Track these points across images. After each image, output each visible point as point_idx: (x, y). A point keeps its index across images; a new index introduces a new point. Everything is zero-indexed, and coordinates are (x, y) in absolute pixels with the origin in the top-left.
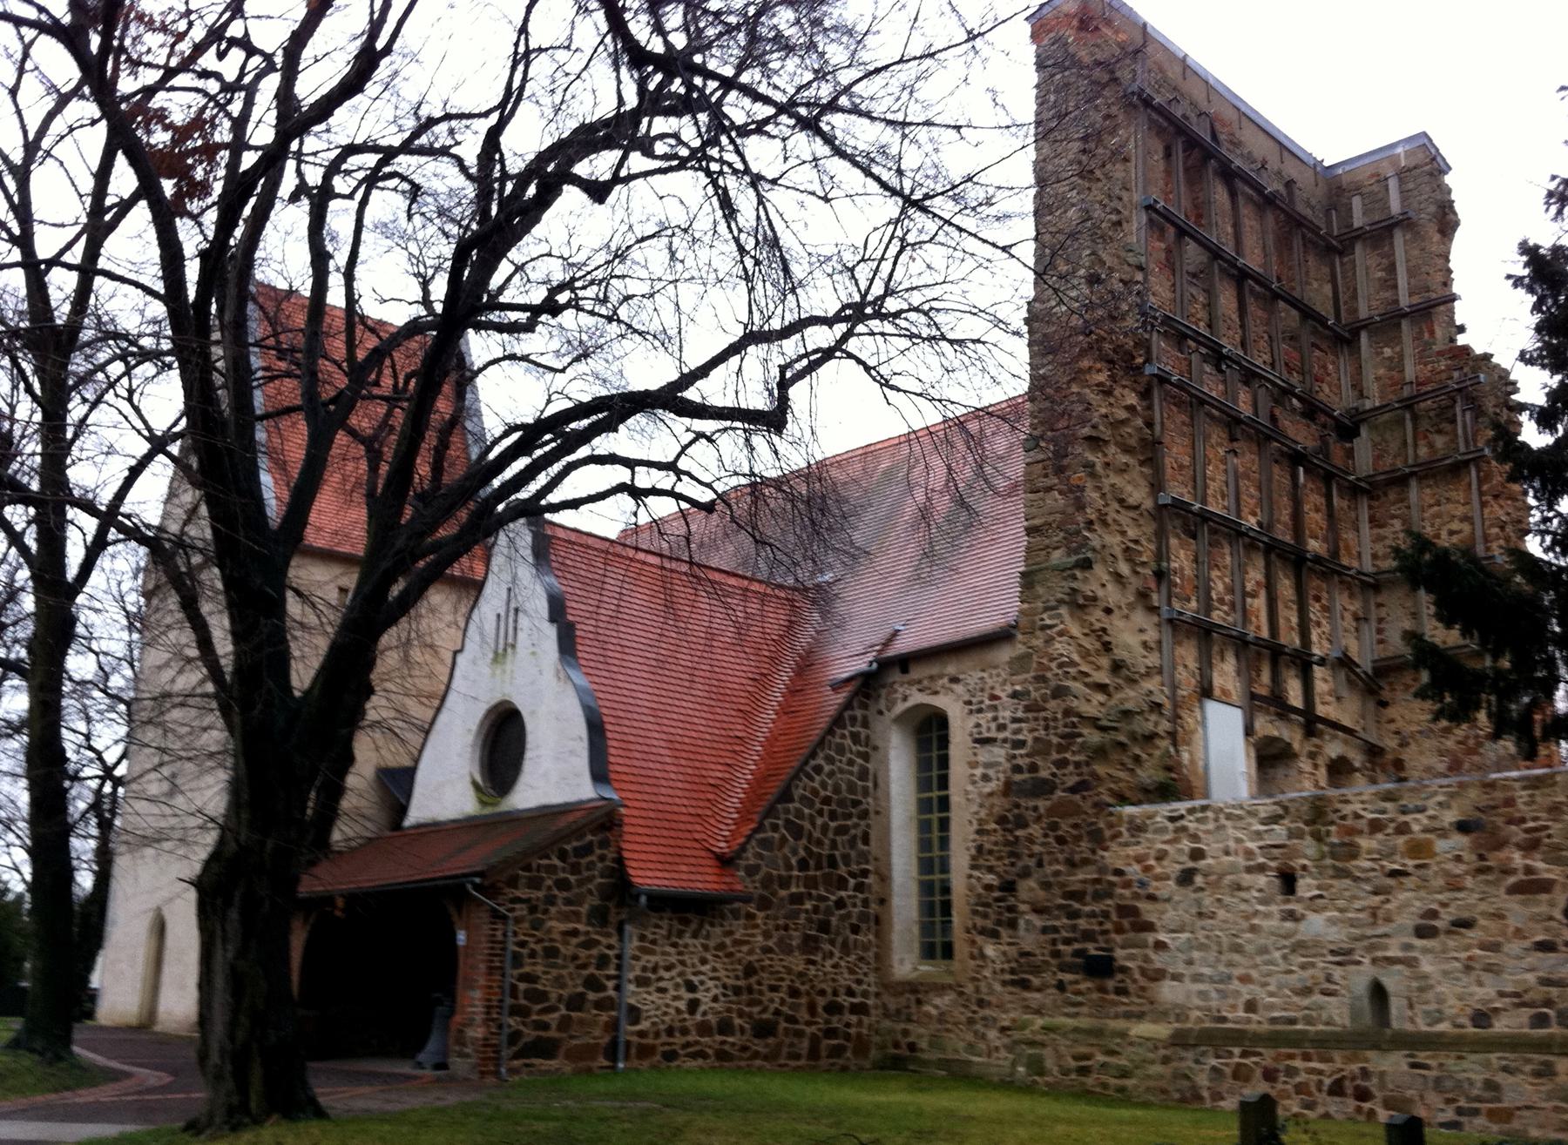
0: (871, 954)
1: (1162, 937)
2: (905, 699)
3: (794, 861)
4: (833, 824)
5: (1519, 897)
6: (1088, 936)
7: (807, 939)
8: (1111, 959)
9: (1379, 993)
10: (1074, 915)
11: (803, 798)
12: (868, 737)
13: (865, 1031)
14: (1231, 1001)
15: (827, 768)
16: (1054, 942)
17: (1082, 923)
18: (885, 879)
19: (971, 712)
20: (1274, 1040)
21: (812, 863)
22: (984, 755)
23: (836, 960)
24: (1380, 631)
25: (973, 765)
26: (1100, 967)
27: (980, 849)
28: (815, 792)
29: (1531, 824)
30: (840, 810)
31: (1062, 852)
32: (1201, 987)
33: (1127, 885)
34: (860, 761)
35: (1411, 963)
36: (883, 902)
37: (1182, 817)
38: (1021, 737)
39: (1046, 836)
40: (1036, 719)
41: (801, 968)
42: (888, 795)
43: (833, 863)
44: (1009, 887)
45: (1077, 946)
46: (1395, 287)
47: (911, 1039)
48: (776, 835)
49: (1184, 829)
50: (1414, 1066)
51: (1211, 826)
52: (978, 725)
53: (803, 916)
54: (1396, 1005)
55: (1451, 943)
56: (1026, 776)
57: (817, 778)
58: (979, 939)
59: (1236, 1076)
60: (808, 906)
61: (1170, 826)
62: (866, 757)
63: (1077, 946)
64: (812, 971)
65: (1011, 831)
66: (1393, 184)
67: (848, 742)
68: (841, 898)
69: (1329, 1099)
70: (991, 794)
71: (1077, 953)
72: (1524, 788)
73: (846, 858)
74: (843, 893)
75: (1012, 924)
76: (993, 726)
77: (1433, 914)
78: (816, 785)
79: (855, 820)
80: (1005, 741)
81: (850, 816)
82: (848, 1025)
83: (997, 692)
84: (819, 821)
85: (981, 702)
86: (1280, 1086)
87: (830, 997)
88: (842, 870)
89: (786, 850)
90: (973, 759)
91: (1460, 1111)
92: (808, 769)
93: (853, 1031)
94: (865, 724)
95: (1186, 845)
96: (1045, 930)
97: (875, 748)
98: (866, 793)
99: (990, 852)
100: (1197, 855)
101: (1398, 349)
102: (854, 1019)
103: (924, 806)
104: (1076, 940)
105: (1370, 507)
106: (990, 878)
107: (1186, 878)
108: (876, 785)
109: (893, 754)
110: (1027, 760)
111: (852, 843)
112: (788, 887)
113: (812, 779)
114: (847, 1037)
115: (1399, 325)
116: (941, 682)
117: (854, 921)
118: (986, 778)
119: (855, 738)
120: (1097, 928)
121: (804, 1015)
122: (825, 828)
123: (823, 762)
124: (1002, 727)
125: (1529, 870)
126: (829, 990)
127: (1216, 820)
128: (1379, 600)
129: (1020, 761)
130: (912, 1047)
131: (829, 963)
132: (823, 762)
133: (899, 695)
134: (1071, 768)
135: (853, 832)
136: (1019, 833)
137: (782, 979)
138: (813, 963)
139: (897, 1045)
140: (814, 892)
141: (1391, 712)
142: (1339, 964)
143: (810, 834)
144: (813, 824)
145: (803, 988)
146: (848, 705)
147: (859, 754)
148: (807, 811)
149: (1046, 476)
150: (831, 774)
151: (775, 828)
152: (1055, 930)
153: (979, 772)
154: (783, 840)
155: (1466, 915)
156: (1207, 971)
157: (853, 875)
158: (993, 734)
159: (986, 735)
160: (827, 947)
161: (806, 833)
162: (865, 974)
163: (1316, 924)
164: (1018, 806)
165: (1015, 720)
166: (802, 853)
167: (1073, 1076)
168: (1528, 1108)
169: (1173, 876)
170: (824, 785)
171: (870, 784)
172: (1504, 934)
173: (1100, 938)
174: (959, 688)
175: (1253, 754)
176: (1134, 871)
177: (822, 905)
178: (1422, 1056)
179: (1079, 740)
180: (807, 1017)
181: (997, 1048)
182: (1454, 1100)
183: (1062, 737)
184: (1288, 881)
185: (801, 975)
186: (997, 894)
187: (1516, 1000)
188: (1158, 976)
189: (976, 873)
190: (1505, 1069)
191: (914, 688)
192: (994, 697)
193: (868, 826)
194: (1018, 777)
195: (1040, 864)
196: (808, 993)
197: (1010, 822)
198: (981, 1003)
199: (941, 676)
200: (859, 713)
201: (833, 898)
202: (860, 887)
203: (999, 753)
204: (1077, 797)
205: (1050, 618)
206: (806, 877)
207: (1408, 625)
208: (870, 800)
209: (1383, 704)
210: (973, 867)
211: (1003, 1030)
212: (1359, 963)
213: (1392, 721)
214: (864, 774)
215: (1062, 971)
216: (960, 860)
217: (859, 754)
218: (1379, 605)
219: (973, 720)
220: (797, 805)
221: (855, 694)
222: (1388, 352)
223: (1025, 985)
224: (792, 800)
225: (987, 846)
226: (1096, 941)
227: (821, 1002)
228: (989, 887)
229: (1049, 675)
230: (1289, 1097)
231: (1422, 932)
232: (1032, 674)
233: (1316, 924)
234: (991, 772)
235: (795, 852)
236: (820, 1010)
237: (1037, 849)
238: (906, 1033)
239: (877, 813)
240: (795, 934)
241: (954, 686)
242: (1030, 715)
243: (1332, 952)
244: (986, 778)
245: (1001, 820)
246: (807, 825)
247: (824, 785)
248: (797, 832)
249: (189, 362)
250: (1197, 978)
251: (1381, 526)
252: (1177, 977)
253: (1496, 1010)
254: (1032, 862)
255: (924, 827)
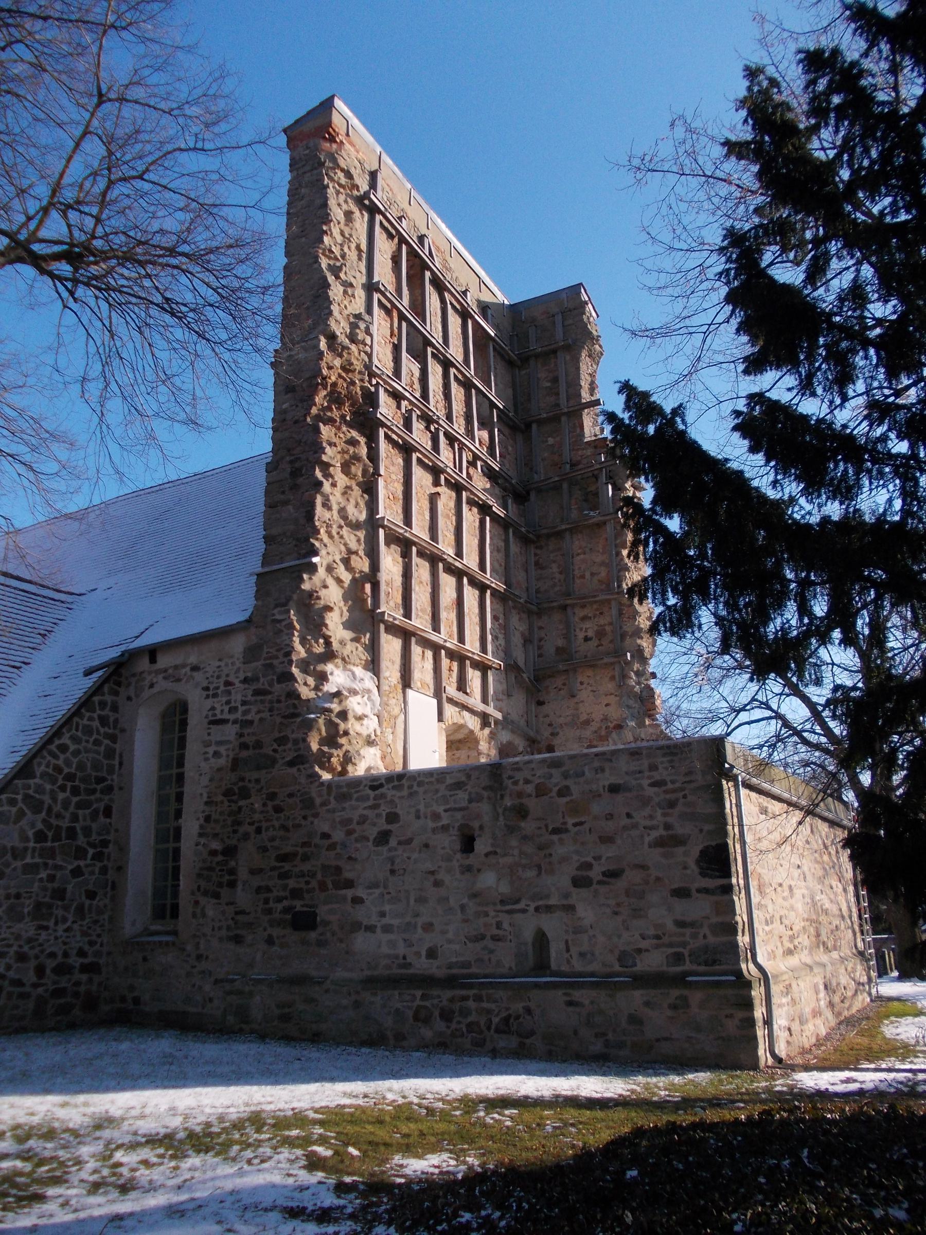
0: (106, 916)
1: (360, 892)
2: (152, 686)
3: (30, 834)
4: (75, 799)
5: (659, 850)
6: (296, 894)
7: (38, 905)
8: (315, 915)
9: (541, 940)
10: (284, 876)
11: (44, 775)
12: (116, 721)
13: (94, 988)
14: (415, 949)
15: (72, 747)
16: (266, 901)
17: (292, 883)
18: (123, 849)
19: (208, 697)
20: (451, 982)
21: (50, 834)
22: (217, 733)
23: (69, 924)
24: (540, 648)
25: (208, 744)
26: (304, 922)
27: (208, 819)
28: (58, 769)
29: (670, 786)
30: (82, 786)
31: (278, 819)
32: (391, 937)
33: (332, 847)
34: (107, 742)
35: (571, 908)
36: (119, 869)
37: (381, 786)
38: (249, 717)
39: (264, 805)
40: (262, 702)
41: (32, 932)
42: (131, 773)
43: (72, 833)
44: (230, 851)
45: (286, 903)
46: (558, 394)
47: (136, 994)
48: (14, 810)
49: (383, 796)
50: (570, 1003)
51: (405, 792)
52: (213, 708)
53: (36, 884)
54: (555, 949)
55: (602, 889)
56: (250, 752)
57: (62, 757)
58: (203, 900)
59: (416, 1018)
60: (43, 875)
61: (372, 794)
62: (113, 738)
63: (286, 903)
64: (44, 935)
65: (236, 802)
66: (559, 318)
67: (96, 724)
68: (79, 867)
69: (496, 1036)
70: (219, 770)
71: (286, 910)
72: (664, 755)
73: (87, 831)
74: (82, 863)
75: (232, 884)
76: (226, 708)
77: (589, 866)
78: (60, 762)
79: (98, 795)
80: (235, 722)
81: (94, 791)
82: (78, 984)
83: (231, 678)
84: (61, 796)
85: (218, 688)
86: (454, 1026)
87: (60, 959)
88: (81, 840)
89: (24, 823)
90: (207, 738)
91: (607, 1044)
92: (53, 747)
93: (82, 989)
94: (115, 708)
95: (384, 809)
96: (259, 890)
97: (123, 731)
98: (111, 770)
99: (216, 821)
100: (392, 818)
101: (558, 439)
102: (84, 977)
103: (163, 782)
104: (286, 898)
105: (536, 555)
106: (216, 845)
107: (383, 838)
108: (121, 764)
109: (138, 736)
110: (254, 738)
111: (94, 816)
112: (23, 859)
113: (55, 757)
114: (76, 994)
115: (560, 421)
116: (184, 671)
117: (90, 887)
118: (216, 754)
119: (103, 721)
120: (303, 886)
121: (31, 977)
122: (66, 804)
123: (68, 742)
124: (233, 710)
125: (667, 827)
126: (60, 953)
127: (410, 787)
128: (540, 624)
129: (246, 739)
130: (136, 1001)
131: (61, 927)
132: (68, 742)
133: (147, 683)
134: (290, 745)
135: (95, 806)
136: (241, 803)
137: (10, 946)
138: (46, 928)
139: (123, 999)
140: (50, 862)
141: (545, 709)
142: (509, 912)
143: (50, 810)
144: (54, 799)
145: (32, 953)
146: (97, 690)
147: (107, 736)
148: (48, 787)
149: (283, 492)
150: (77, 753)
151: (12, 802)
152: (268, 889)
153: (211, 750)
154: (21, 814)
155: (612, 867)
156: (396, 922)
157: (93, 846)
158: (226, 716)
159: (219, 717)
160: (60, 912)
161: (46, 806)
162: (99, 936)
163: (488, 880)
164: (242, 779)
165: (244, 703)
166: (40, 826)
167: (275, 1023)
168: (666, 1039)
169: (372, 838)
170: (68, 763)
171: (116, 762)
172: (647, 883)
173: (306, 895)
174: (198, 676)
175: (444, 739)
176: (338, 835)
177: (59, 874)
178: (577, 995)
179: (299, 720)
180: (34, 979)
181: (211, 1000)
182: (604, 1034)
183: (285, 717)
184: (468, 844)
185: (30, 941)
186: (220, 858)
187: (655, 941)
188: (356, 926)
189: (203, 841)
190: (647, 1004)
191: (161, 676)
192: (228, 683)
193: (111, 800)
194: (244, 754)
195: (259, 831)
196: (37, 957)
197: (236, 793)
198: (199, 957)
199: (184, 666)
200: (108, 698)
201: (70, 867)
202: (98, 856)
203: (230, 731)
204: (294, 770)
205: (280, 613)
206: (42, 849)
207: (560, 643)
208: (115, 777)
209: (540, 703)
210: (201, 835)
211: (216, 982)
212: (524, 911)
213: (547, 716)
214: (110, 754)
215: (271, 926)
216: (190, 826)
217: (107, 736)
218: (540, 628)
219: (209, 703)
220: (37, 781)
221: (105, 681)
222: (551, 441)
223: (238, 940)
224: (35, 777)
225: (214, 816)
226: (302, 899)
227: (50, 964)
228: (213, 853)
229: (275, 662)
230: (462, 1035)
231: (579, 882)
232: (262, 662)
233: (488, 880)
234: (222, 749)
235: (33, 825)
236: (48, 971)
237: (257, 817)
238: (132, 988)
239: (121, 788)
240: (28, 902)
241: (195, 674)
242: (259, 698)
243: (502, 902)
244: (216, 754)
245: (228, 793)
246: (47, 799)
247: (68, 763)
248: (37, 807)
249: (420, 784)
250: (387, 929)
251: (542, 568)
252: (371, 929)
253: (639, 951)
254: (251, 829)
255: (162, 801)
